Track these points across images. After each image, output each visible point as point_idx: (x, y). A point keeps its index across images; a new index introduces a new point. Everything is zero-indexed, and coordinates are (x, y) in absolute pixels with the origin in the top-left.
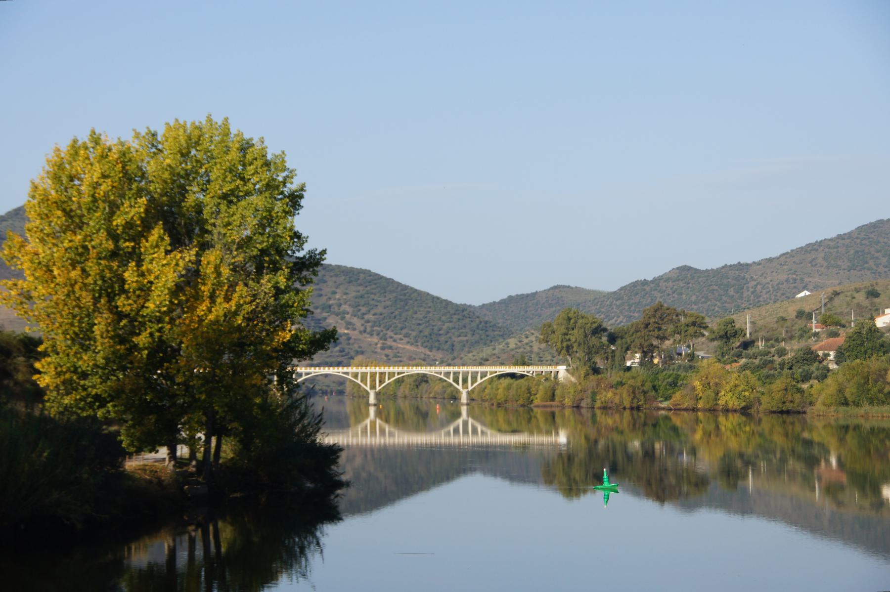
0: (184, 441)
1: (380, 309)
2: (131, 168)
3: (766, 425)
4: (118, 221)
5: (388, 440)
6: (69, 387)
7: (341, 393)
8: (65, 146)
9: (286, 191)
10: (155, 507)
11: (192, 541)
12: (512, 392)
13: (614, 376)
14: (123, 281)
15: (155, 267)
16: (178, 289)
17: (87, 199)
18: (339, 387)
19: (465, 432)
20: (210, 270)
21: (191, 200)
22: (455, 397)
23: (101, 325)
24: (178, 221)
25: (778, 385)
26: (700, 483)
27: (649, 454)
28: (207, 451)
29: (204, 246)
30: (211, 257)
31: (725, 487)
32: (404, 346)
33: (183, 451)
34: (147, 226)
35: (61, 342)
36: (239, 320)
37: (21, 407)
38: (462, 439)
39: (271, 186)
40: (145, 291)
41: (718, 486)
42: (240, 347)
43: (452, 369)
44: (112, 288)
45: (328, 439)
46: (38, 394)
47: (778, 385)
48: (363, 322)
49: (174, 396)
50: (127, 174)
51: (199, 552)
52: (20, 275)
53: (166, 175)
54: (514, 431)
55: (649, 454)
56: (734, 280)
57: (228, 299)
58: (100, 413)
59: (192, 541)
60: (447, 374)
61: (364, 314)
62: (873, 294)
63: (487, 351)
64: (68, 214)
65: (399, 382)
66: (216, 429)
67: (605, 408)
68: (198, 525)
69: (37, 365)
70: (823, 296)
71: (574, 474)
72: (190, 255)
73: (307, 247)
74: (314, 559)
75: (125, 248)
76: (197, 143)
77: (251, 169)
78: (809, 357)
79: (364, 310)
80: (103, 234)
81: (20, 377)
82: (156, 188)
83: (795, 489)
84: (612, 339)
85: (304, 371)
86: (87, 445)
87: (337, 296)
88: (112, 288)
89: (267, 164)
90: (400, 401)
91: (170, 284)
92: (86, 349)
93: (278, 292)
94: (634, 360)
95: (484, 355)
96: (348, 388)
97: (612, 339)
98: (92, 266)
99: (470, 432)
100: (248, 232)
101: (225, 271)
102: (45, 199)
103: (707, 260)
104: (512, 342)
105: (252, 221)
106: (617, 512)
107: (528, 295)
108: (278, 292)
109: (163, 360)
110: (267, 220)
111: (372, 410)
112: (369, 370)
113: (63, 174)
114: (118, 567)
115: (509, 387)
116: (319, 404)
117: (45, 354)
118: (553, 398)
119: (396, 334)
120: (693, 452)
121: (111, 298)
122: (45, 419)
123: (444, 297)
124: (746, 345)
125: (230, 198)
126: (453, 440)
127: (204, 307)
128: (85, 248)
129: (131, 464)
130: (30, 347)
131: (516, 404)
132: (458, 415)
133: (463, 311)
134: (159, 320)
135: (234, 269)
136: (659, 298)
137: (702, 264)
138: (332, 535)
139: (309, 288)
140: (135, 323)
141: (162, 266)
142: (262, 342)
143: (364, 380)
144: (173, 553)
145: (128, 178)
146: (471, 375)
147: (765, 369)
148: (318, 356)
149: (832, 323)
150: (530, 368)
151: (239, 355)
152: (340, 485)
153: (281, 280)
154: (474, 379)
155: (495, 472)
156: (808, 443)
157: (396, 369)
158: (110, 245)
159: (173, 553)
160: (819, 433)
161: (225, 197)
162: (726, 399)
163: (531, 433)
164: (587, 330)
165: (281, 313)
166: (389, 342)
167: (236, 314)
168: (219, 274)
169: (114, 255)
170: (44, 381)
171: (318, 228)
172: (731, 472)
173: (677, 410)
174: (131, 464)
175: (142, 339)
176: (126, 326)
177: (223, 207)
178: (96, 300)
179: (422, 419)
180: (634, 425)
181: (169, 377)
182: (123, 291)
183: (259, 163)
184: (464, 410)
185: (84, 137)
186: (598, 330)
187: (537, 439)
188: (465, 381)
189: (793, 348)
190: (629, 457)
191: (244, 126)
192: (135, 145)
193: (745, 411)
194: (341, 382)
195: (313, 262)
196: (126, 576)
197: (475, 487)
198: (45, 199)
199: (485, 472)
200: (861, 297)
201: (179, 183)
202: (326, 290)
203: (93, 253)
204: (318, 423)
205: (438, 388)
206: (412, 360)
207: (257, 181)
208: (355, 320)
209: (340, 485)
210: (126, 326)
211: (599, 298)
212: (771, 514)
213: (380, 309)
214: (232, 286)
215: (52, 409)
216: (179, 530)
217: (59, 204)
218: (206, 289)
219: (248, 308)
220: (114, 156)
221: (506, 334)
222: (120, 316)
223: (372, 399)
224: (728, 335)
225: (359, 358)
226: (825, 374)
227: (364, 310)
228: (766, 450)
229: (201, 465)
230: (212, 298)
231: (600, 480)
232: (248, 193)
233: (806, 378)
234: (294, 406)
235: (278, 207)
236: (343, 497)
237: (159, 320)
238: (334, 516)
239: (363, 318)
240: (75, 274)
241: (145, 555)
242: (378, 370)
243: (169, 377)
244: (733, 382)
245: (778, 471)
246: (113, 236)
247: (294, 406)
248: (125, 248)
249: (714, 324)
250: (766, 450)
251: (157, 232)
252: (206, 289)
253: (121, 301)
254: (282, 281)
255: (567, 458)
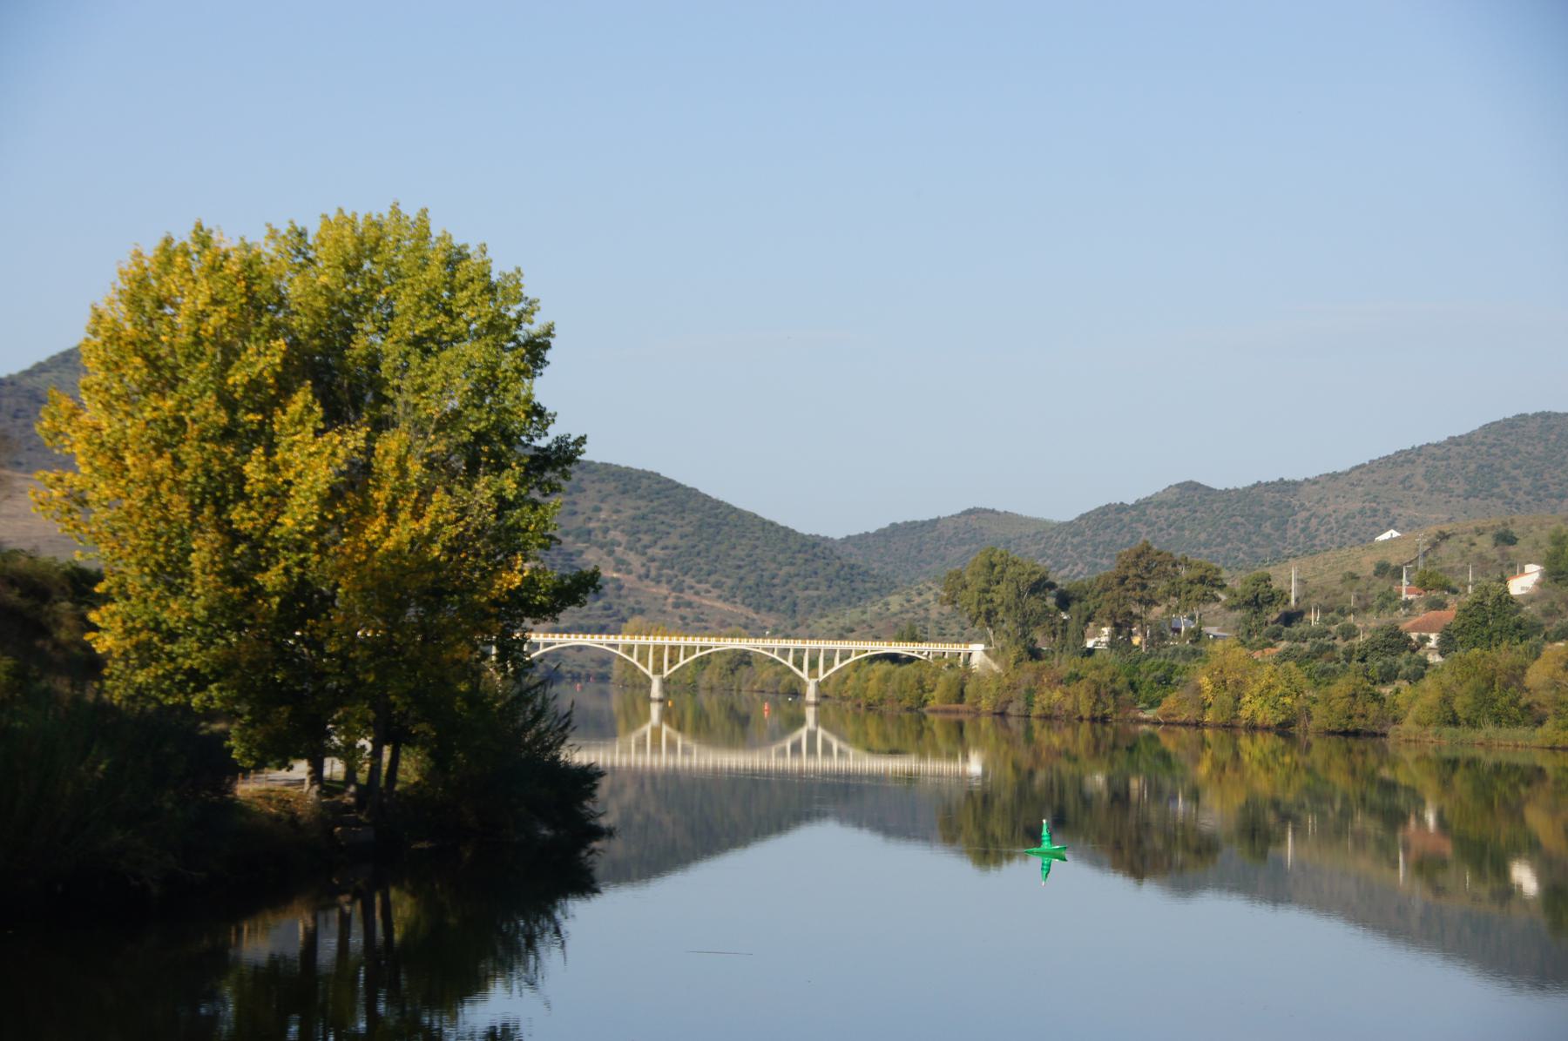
0: (336, 752)
1: (673, 540)
2: (261, 289)
3: (1318, 754)
4: (237, 377)
5: (680, 761)
6: (146, 653)
7: (604, 678)
8: (150, 248)
9: (522, 335)
10: (285, 860)
11: (345, 920)
12: (893, 686)
13: (1065, 664)
14: (242, 479)
15: (296, 457)
16: (334, 496)
17: (185, 339)
18: (600, 669)
19: (656, 746)
20: (389, 465)
21: (360, 345)
22: (796, 691)
23: (202, 551)
24: (337, 380)
25: (1341, 686)
26: (1205, 848)
27: (1120, 797)
28: (375, 770)
29: (381, 425)
30: (391, 443)
31: (1249, 854)
32: (713, 603)
33: (334, 768)
34: (285, 388)
35: (135, 579)
36: (436, 551)
37: (63, 686)
38: (806, 763)
39: (497, 327)
40: (278, 497)
41: (1234, 854)
42: (435, 596)
43: (791, 644)
44: (222, 490)
45: (579, 755)
46: (93, 665)
47: (1341, 686)
48: (644, 559)
49: (321, 676)
50: (255, 299)
51: (357, 940)
52: (68, 463)
53: (320, 303)
54: (894, 752)
55: (1120, 797)
56: (1271, 508)
57: (417, 515)
58: (196, 701)
59: (345, 920)
60: (784, 652)
61: (646, 547)
62: (1506, 538)
63: (852, 615)
64: (152, 363)
65: (703, 662)
66: (391, 733)
67: (1048, 718)
68: (357, 894)
69: (93, 616)
70: (1421, 539)
71: (994, 826)
72: (356, 438)
73: (554, 431)
74: (550, 957)
75: (247, 424)
76: (374, 250)
77: (463, 297)
78: (1395, 641)
79: (646, 539)
80: (210, 398)
81: (63, 635)
82: (302, 323)
83: (1364, 864)
84: (1064, 601)
85: (543, 640)
86: (172, 754)
87: (603, 516)
88: (222, 490)
89: (491, 289)
90: (703, 696)
91: (322, 487)
92: (176, 591)
93: (503, 505)
94: (1099, 638)
95: (846, 621)
96: (616, 671)
97: (1064, 601)
98: (191, 454)
99: (820, 751)
100: (455, 403)
101: (415, 468)
102: (115, 337)
103: (1228, 473)
104: (895, 602)
105: (463, 385)
106: (1062, 894)
107: (923, 524)
108: (503, 505)
109: (305, 614)
110: (488, 384)
111: (655, 709)
112: (652, 641)
113: (145, 297)
114: (220, 961)
115: (887, 678)
116: (565, 696)
117: (107, 598)
118: (960, 697)
119: (700, 582)
120: (1195, 795)
121: (220, 508)
122: (103, 709)
123: (781, 521)
124: (1289, 618)
125: (425, 344)
126: (790, 763)
127: (376, 527)
128: (180, 421)
129: (247, 789)
130: (81, 585)
131: (899, 707)
132: (800, 721)
133: (814, 548)
134: (302, 547)
135: (431, 464)
136: (1144, 535)
137: (1220, 480)
138: (585, 920)
139: (554, 500)
140: (260, 549)
141: (309, 457)
142: (473, 589)
143: (643, 657)
144: (311, 940)
145: (256, 306)
146: (824, 654)
147: (1320, 660)
148: (568, 615)
149: (1435, 585)
150: (924, 647)
151: (433, 610)
152: (598, 833)
153: (509, 485)
154: (829, 662)
155: (859, 819)
156: (1389, 787)
157: (698, 642)
158: (222, 418)
159: (311, 940)
160: (1408, 771)
161: (417, 342)
162: (1254, 707)
163: (922, 755)
164: (1022, 586)
165: (508, 541)
166: (688, 596)
167: (430, 540)
168: (403, 472)
169: (227, 434)
170: (104, 643)
171: (575, 400)
172: (1257, 832)
173: (1169, 724)
174: (247, 789)
175: (271, 578)
176: (245, 556)
177: (414, 360)
178: (195, 510)
179: (739, 727)
180: (1096, 747)
181: (315, 643)
182: (241, 496)
183: (477, 286)
184: (810, 713)
185: (183, 235)
186: (1041, 586)
187: (932, 766)
188: (813, 665)
189: (1368, 626)
190: (1086, 801)
191: (456, 224)
192: (269, 250)
193: (1284, 730)
194: (605, 660)
195: (564, 456)
196: (232, 977)
197: (824, 844)
198: (115, 337)
199: (842, 819)
200: (1485, 544)
201: (341, 317)
202: (585, 504)
203: (193, 431)
204: (564, 727)
205: (767, 674)
206: (724, 627)
207: (473, 316)
208: (631, 557)
209: (598, 833)
210: (245, 556)
211: (1044, 531)
212: (1322, 904)
213: (673, 540)
214: (426, 493)
215: (116, 691)
216: (323, 901)
217: (137, 347)
218: (381, 497)
219: (451, 531)
220: (233, 267)
221: (885, 587)
222: (235, 537)
223: (656, 691)
224: (1259, 600)
225: (636, 621)
226: (1420, 671)
227: (646, 539)
228: (1318, 796)
229: (364, 793)
230: (392, 511)
231: (1034, 837)
232: (457, 338)
233: (1389, 676)
234: (523, 698)
235: (508, 362)
236: (602, 854)
237: (302, 547)
238: (585, 885)
239: (644, 554)
240: (160, 465)
241: (266, 941)
242: (667, 641)
243: (315, 643)
244: (1267, 681)
245: (1336, 832)
246: (227, 402)
247: (523, 698)
248: (247, 424)
249: (1236, 581)
250: (1318, 796)
251: (302, 398)
252: (381, 497)
253: (237, 513)
254: (510, 486)
255: (982, 799)
